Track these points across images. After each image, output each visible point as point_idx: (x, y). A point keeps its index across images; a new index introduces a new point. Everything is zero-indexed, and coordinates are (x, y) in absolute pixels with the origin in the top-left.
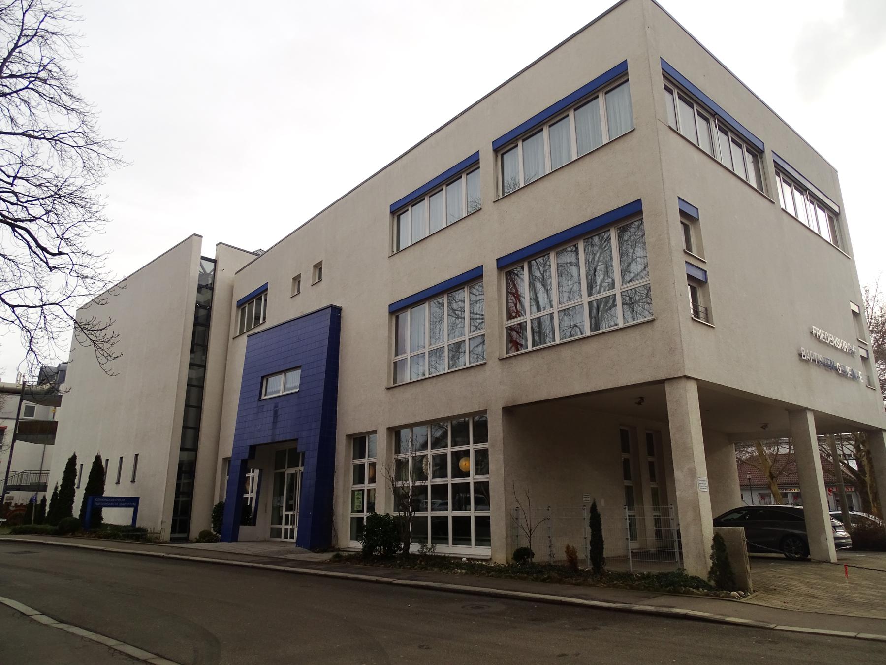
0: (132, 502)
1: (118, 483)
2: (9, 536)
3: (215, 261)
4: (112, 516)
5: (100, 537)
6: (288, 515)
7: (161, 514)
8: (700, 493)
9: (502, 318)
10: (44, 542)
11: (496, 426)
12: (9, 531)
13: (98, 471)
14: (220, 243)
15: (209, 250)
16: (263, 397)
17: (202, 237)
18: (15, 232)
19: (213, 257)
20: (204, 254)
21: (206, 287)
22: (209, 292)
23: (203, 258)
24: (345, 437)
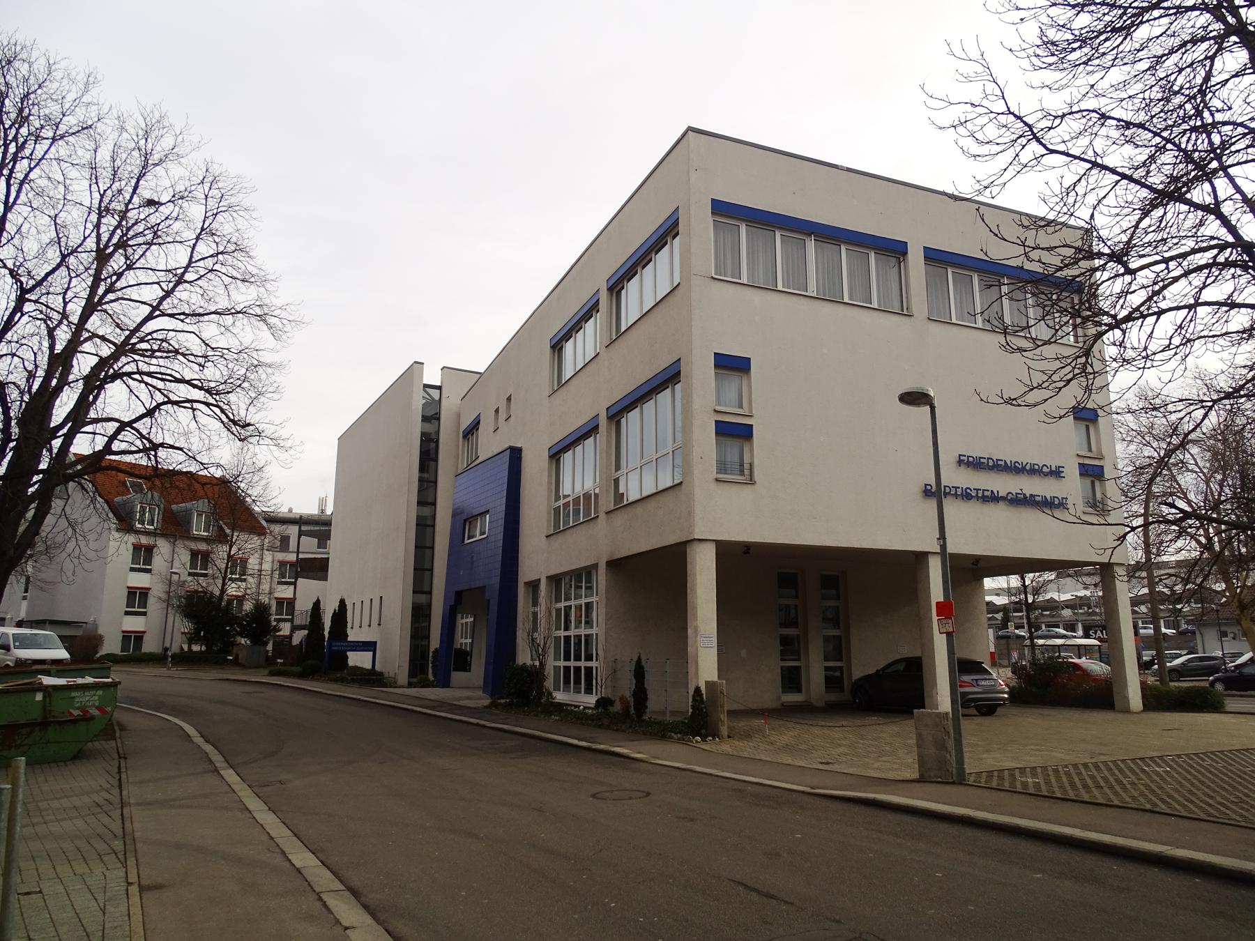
0: (370, 646)
1: (370, 626)
2: (268, 678)
3: (439, 388)
4: (358, 659)
5: (341, 680)
6: (575, 660)
7: (398, 659)
8: (699, 648)
9: (611, 470)
10: (282, 683)
11: (602, 577)
12: (266, 671)
13: (340, 615)
14: (444, 367)
15: (432, 376)
16: (467, 541)
17: (423, 364)
18: (211, 407)
19: (438, 384)
20: (426, 381)
21: (432, 416)
22: (436, 422)
23: (426, 386)
24: (523, 584)
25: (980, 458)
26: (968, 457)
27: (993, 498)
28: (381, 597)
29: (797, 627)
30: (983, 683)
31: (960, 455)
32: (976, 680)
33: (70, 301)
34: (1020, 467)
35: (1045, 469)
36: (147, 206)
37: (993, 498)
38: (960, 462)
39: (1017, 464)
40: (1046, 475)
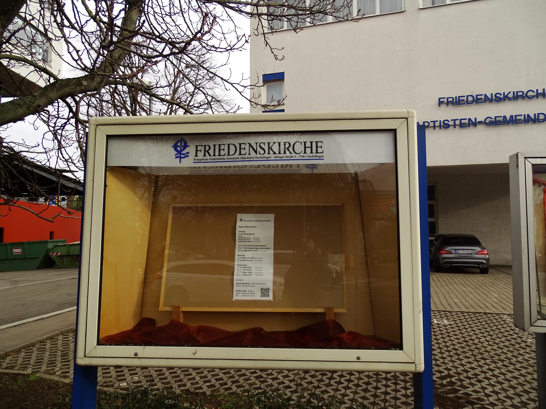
18: (250, 147)
25: (459, 97)
26: (448, 98)
27: (473, 123)
28: (180, 162)
29: (434, 217)
30: (461, 252)
31: (440, 99)
32: (455, 250)
33: (51, 16)
34: (502, 96)
35: (530, 94)
36: (186, 68)
37: (473, 123)
38: (440, 103)
39: (498, 95)
40: (532, 97)
